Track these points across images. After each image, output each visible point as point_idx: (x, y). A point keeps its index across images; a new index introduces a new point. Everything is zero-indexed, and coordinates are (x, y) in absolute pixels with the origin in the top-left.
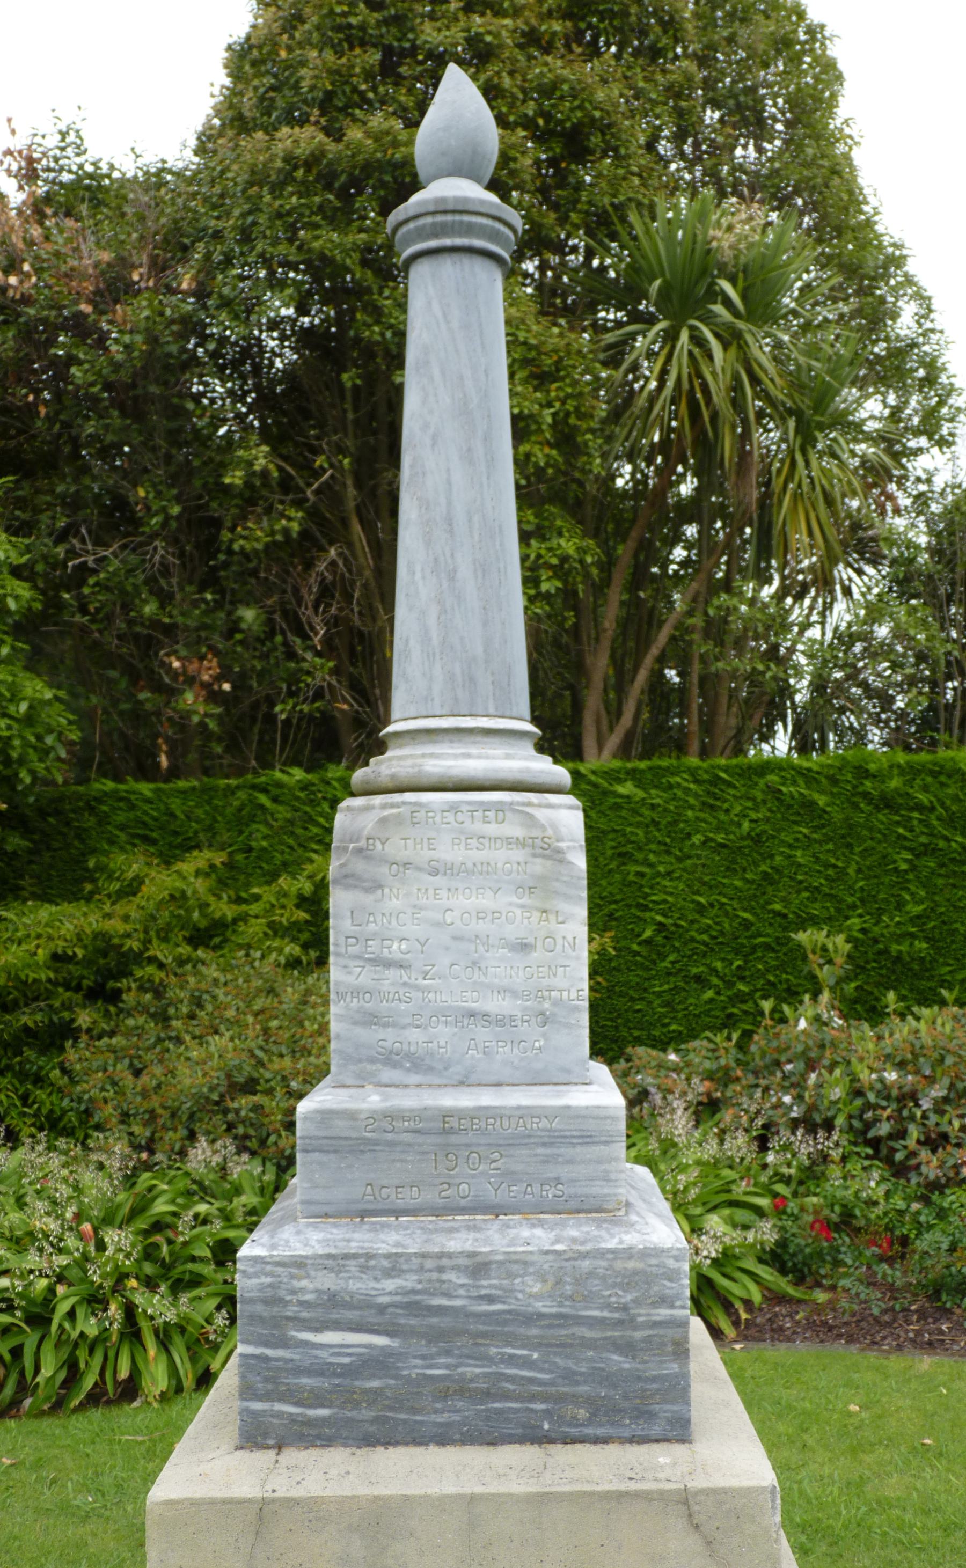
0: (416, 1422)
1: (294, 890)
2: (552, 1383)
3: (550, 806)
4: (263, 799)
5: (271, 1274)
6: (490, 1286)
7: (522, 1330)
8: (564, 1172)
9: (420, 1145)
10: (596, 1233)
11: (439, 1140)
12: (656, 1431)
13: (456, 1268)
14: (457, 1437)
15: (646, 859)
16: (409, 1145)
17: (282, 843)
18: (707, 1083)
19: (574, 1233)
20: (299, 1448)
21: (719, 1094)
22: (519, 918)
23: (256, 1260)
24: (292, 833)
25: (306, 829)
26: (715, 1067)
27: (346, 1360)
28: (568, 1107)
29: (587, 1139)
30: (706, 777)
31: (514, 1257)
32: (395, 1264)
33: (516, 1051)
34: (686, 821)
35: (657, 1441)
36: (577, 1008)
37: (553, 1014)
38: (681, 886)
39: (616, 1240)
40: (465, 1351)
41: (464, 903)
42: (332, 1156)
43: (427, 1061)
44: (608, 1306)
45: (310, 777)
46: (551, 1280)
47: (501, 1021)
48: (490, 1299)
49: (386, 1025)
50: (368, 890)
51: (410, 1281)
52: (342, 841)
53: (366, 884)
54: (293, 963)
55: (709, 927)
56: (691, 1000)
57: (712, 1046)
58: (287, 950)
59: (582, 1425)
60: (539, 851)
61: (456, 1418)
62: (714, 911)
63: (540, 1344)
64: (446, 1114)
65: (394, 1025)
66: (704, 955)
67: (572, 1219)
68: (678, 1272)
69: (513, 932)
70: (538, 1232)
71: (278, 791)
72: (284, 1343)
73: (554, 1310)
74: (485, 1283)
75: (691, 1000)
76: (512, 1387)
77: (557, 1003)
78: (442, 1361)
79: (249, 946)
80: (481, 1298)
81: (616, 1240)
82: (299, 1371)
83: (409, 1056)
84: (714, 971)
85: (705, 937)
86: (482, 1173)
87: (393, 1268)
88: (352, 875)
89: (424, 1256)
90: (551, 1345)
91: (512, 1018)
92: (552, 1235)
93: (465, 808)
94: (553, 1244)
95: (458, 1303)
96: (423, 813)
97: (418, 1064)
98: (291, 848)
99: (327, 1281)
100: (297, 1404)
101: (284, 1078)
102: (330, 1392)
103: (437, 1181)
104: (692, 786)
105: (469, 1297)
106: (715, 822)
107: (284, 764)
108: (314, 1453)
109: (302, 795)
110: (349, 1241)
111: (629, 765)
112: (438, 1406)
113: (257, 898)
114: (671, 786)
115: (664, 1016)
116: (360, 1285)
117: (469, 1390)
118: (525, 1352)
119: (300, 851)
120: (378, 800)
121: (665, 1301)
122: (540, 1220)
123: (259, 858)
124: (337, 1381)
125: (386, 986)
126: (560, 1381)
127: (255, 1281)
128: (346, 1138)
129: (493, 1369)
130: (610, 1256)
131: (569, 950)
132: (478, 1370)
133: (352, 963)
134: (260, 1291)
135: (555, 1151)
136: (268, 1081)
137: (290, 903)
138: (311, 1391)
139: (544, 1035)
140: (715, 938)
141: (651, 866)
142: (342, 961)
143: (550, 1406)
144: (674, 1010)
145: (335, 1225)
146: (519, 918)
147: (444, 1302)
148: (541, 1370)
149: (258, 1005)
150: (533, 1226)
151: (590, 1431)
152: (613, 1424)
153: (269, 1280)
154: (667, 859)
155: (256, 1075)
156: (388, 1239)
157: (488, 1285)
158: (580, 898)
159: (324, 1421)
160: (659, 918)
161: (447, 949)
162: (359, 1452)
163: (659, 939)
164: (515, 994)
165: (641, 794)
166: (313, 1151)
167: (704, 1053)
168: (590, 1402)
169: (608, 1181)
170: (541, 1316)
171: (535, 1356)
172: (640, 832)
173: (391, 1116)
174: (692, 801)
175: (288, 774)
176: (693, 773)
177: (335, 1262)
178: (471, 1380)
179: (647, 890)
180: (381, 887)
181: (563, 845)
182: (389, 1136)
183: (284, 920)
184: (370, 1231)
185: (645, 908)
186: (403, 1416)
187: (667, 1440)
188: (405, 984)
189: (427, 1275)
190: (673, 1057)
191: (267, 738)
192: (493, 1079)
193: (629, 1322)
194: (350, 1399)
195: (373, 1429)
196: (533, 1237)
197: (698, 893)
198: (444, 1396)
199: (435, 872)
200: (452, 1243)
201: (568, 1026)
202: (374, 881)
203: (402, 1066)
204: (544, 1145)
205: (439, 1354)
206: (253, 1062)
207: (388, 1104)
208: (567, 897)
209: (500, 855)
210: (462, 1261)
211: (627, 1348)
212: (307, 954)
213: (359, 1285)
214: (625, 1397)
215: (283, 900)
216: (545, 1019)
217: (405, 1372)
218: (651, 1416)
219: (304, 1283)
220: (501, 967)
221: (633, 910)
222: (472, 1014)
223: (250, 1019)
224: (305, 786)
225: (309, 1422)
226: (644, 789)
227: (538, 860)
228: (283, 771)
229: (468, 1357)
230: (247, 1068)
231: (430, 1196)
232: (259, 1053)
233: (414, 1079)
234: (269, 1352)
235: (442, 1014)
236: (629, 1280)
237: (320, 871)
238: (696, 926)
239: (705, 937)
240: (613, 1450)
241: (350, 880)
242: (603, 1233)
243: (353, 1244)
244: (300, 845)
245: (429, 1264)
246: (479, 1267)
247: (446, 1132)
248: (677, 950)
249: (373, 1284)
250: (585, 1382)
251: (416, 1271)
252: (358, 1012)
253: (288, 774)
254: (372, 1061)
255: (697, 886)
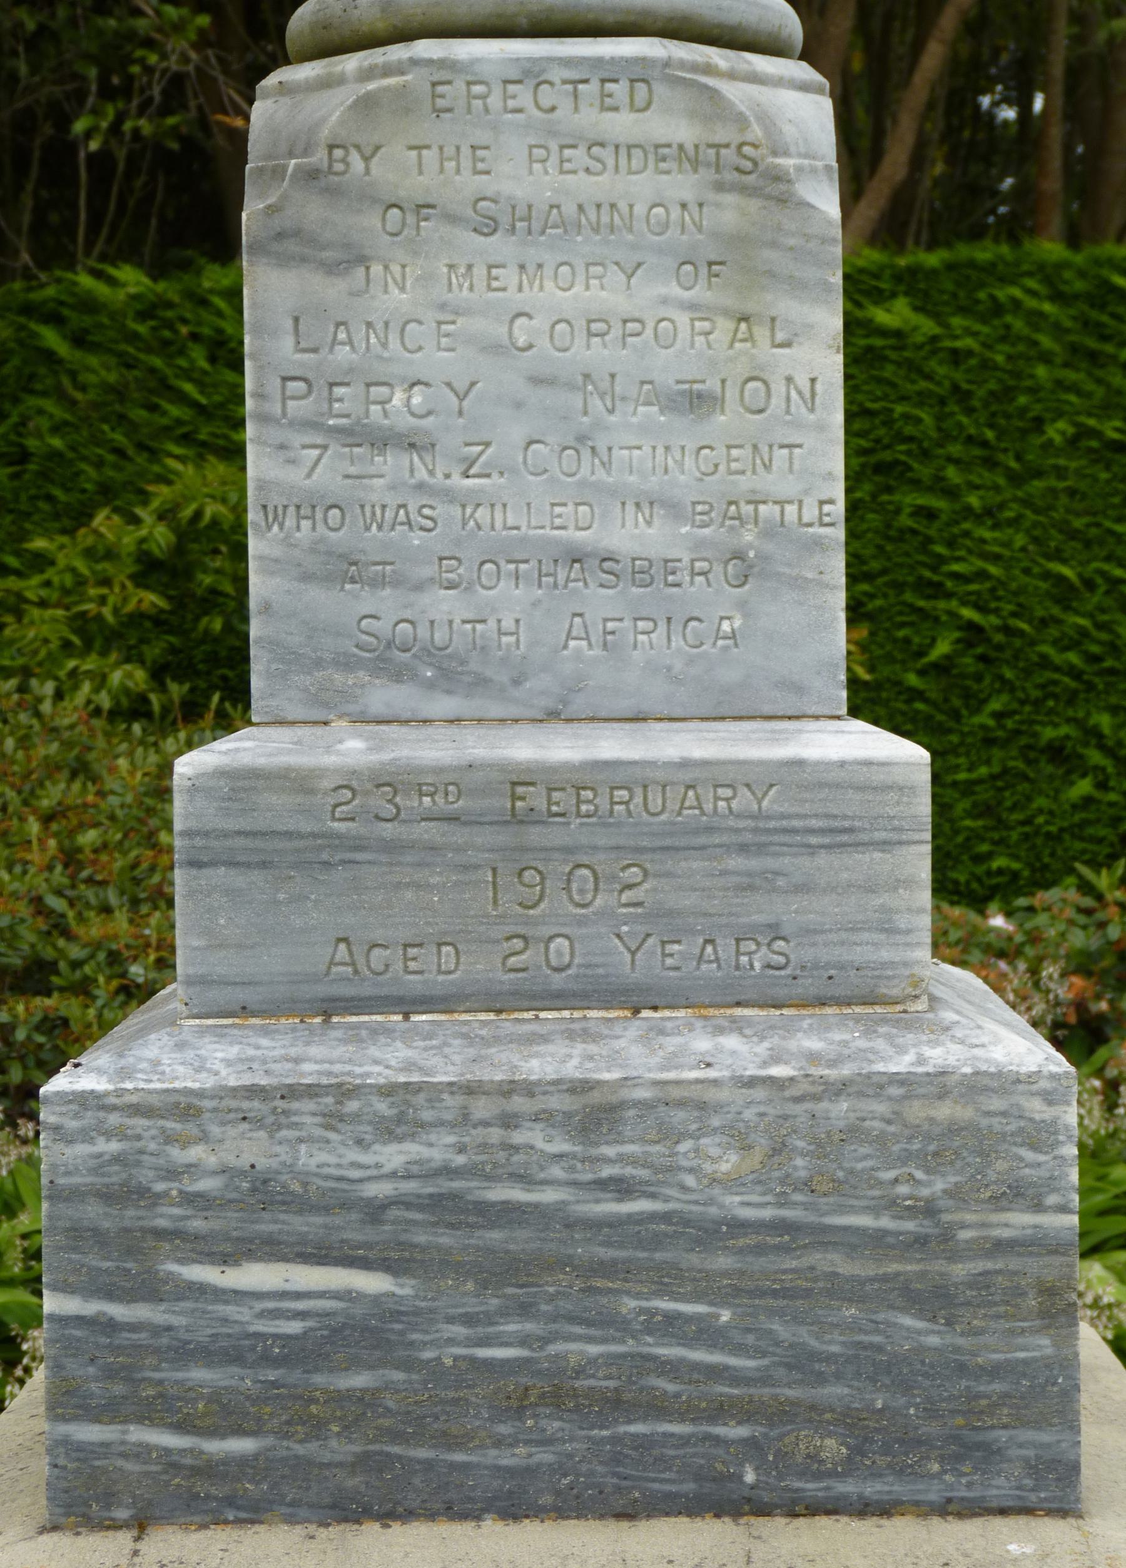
0: (453, 1466)
1: (129, 541)
2: (764, 1379)
3: (755, 78)
4: (51, 338)
5: (120, 1133)
6: (621, 1159)
7: (694, 1259)
8: (789, 911)
9: (459, 850)
10: (862, 1044)
11: (502, 837)
12: (1000, 1488)
13: (543, 1117)
14: (546, 1499)
15: (939, 479)
16: (432, 848)
17: (97, 440)
18: (1077, 981)
19: (814, 1044)
20: (185, 1526)
21: (1104, 1006)
22: (684, 333)
23: (84, 1100)
24: (122, 417)
25: (153, 408)
26: (1095, 943)
27: (294, 1327)
28: (799, 763)
29: (842, 836)
30: (1079, 286)
31: (676, 1093)
32: (403, 1109)
33: (677, 641)
34: (1033, 391)
35: (1003, 1512)
36: (818, 544)
37: (763, 557)
38: (1020, 540)
39: (909, 1058)
40: (565, 1305)
41: (554, 298)
42: (257, 876)
43: (473, 666)
44: (892, 1205)
45: (161, 287)
46: (762, 1144)
47: (644, 572)
48: (622, 1188)
49: (378, 583)
50: (332, 269)
51: (437, 1148)
52: (269, 157)
53: (326, 254)
54: (133, 709)
55: (1084, 633)
56: (1041, 802)
57: (1088, 902)
58: (116, 677)
59: (832, 1474)
60: (730, 176)
61: (545, 1456)
62: (1096, 599)
63: (737, 1291)
64: (519, 779)
65: (397, 582)
66: (1072, 699)
67: (807, 1017)
68: (1052, 1127)
69: (670, 366)
70: (731, 1042)
71: (87, 321)
72: (150, 1290)
73: (767, 1213)
74: (610, 1151)
75: (1041, 802)
76: (671, 1388)
77: (772, 531)
78: (511, 1327)
79: (26, 672)
80: (602, 1184)
81: (909, 1058)
82: (185, 1352)
83: (430, 653)
84: (1096, 734)
85: (1073, 657)
86: (602, 914)
87: (400, 1119)
88: (297, 233)
89: (471, 1089)
90: (763, 1293)
91: (669, 565)
92: (762, 1048)
93: (556, 74)
94: (765, 1064)
95: (548, 1196)
96: (460, 85)
97: (453, 671)
98: (119, 452)
99: (249, 1149)
100: (181, 1427)
101: (114, 958)
102: (255, 1401)
103: (499, 932)
104: (1047, 307)
105: (575, 1184)
106: (1100, 392)
107: (103, 258)
108: (218, 1538)
109: (142, 329)
110: (297, 1061)
111: (902, 262)
112: (503, 1429)
113: (41, 561)
114: (997, 309)
115: (976, 836)
116: (322, 1157)
117: (575, 1394)
118: (701, 1309)
119: (141, 459)
120: (351, 63)
121: (1021, 1194)
122: (733, 1020)
123: (44, 475)
124: (272, 1375)
125: (377, 490)
126: (782, 1371)
127: (81, 1149)
128: (288, 835)
129: (628, 1346)
130: (895, 1091)
131: (798, 407)
132: (594, 1350)
133: (297, 439)
134: (94, 1171)
135: (770, 863)
136: (76, 965)
137: (121, 573)
138: (215, 1397)
139: (742, 605)
140: (1095, 659)
141: (951, 493)
142: (276, 434)
143: (759, 1431)
144: (1001, 824)
145: (265, 1031)
146: (684, 333)
147: (518, 1194)
148: (739, 1349)
149: (51, 796)
150: (720, 1031)
151: (848, 1487)
152: (900, 1472)
153: (115, 1146)
154: (988, 477)
155: (49, 953)
156: (384, 1056)
157: (615, 1155)
158: (828, 288)
159: (243, 1462)
160: (968, 613)
161: (518, 405)
162: (322, 1533)
163: (968, 662)
164: (675, 510)
165: (928, 326)
166: (213, 864)
167: (1070, 913)
168: (848, 1421)
169: (892, 931)
170: (739, 1226)
171: (725, 1316)
172: (926, 416)
173: (390, 782)
174: (1046, 342)
175: (112, 282)
176: (1050, 276)
177: (268, 1104)
178: (579, 1372)
179: (940, 549)
180: (363, 260)
181: (788, 163)
182: (388, 830)
183: (107, 612)
184: (345, 1041)
185: (936, 590)
186: (422, 1453)
187: (1028, 1511)
188: (421, 486)
189: (479, 1134)
190: (998, 921)
191: (54, 218)
192: (624, 706)
193: (940, 1242)
194: (306, 1416)
195: (353, 1482)
196: (721, 1052)
197: (1058, 555)
198: (518, 1406)
199: (488, 227)
200: (535, 1063)
201: (798, 583)
202: (348, 246)
203: (414, 677)
204: (743, 849)
205: (504, 1313)
206: (42, 924)
207: (386, 756)
208: (797, 286)
209: (641, 187)
210: (556, 1102)
211: (936, 1301)
212: (163, 688)
213: (323, 1157)
214: (931, 1412)
215: (105, 566)
216: (743, 568)
217: (427, 1355)
218: (988, 1455)
219: (196, 1153)
220: (643, 448)
221: (908, 597)
222: (577, 559)
223: (34, 827)
224: (149, 310)
225: (210, 1469)
226: (937, 317)
227: (729, 198)
228: (98, 274)
229: (572, 1319)
230: (28, 936)
231: (481, 967)
232: (57, 904)
233: (443, 705)
234: (117, 1311)
235: (507, 556)
236: (939, 1147)
237: (188, 499)
238: (1054, 632)
239: (1073, 657)
240: (901, 1532)
241: (295, 245)
242: (880, 1044)
243: (307, 1067)
244: (141, 446)
245: (482, 1108)
246: (595, 1113)
247: (516, 820)
248: (1008, 686)
249: (354, 1155)
250: (838, 1376)
251: (452, 1125)
252: (313, 550)
253: (112, 282)
254: (347, 664)
255: (1056, 539)
